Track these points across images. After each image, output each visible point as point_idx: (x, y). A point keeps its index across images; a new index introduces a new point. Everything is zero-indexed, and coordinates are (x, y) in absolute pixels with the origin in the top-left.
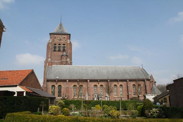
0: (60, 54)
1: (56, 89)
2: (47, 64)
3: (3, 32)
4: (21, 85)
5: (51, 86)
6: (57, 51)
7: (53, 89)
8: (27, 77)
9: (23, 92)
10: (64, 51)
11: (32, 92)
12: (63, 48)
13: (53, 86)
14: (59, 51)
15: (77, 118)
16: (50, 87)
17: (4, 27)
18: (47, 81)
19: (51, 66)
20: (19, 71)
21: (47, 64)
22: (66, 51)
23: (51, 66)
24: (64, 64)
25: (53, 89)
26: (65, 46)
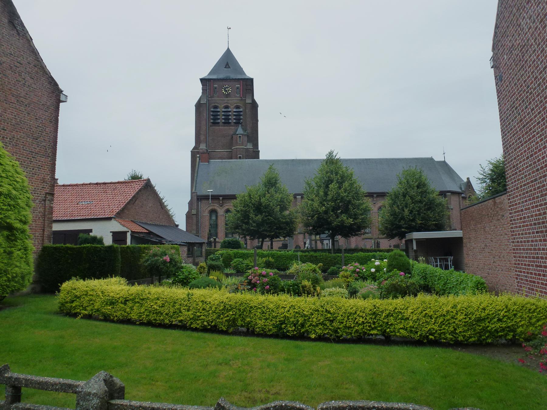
0: (230, 130)
1: (219, 218)
2: (198, 159)
3: (61, 104)
4: (120, 215)
5: (207, 211)
6: (232, 124)
7: (214, 218)
8: (134, 197)
9: (125, 233)
10: (238, 123)
11: (146, 231)
12: (235, 115)
13: (213, 212)
14: (227, 122)
15: (128, 284)
16: (206, 214)
17: (62, 91)
18: (198, 199)
19: (208, 162)
20: (69, 186)
21: (198, 159)
22: (243, 124)
23: (208, 162)
24: (240, 158)
25: (214, 218)
26: (241, 112)
